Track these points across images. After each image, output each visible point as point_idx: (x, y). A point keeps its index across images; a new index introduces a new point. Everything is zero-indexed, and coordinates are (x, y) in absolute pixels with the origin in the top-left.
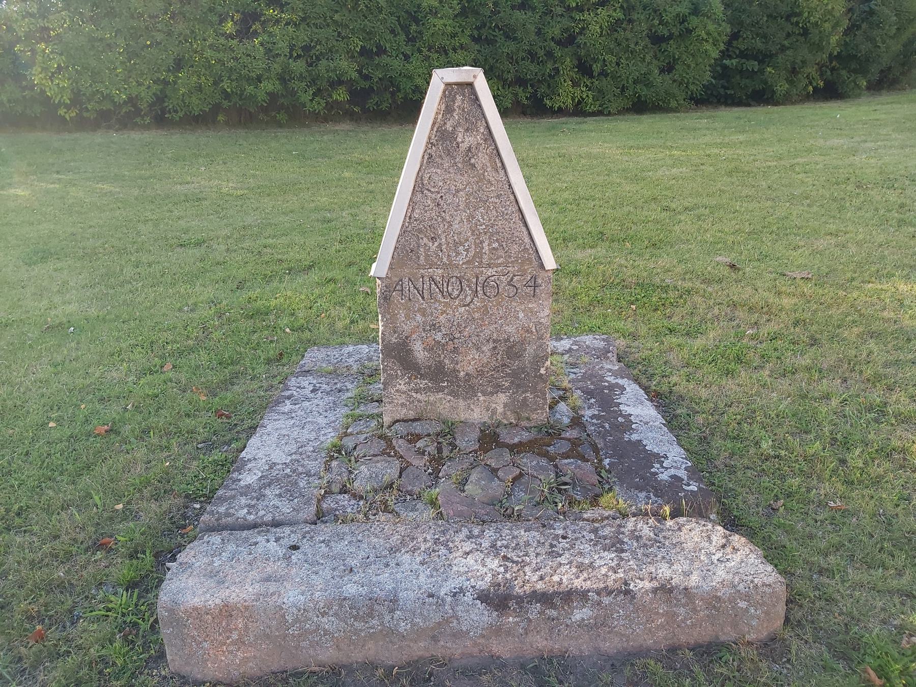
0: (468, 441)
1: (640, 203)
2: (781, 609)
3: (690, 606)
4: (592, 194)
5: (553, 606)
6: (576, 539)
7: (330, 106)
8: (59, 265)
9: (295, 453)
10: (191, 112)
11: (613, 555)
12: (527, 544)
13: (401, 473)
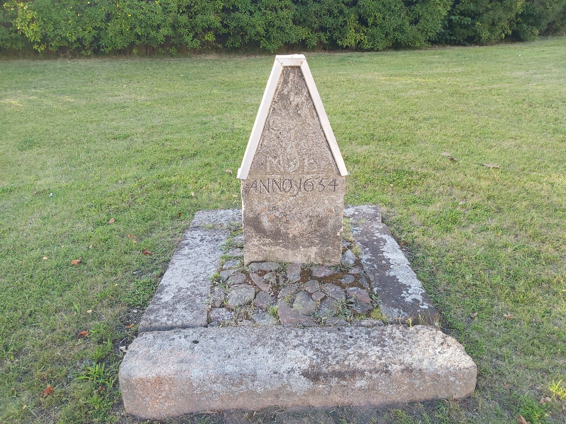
0: (294, 275)
1: (396, 115)
2: (474, 381)
3: (423, 379)
4: (367, 107)
5: (345, 379)
6: (358, 338)
7: (203, 44)
8: (40, 151)
9: (193, 281)
10: (116, 48)
11: (379, 349)
12: (330, 341)
13: (255, 295)
